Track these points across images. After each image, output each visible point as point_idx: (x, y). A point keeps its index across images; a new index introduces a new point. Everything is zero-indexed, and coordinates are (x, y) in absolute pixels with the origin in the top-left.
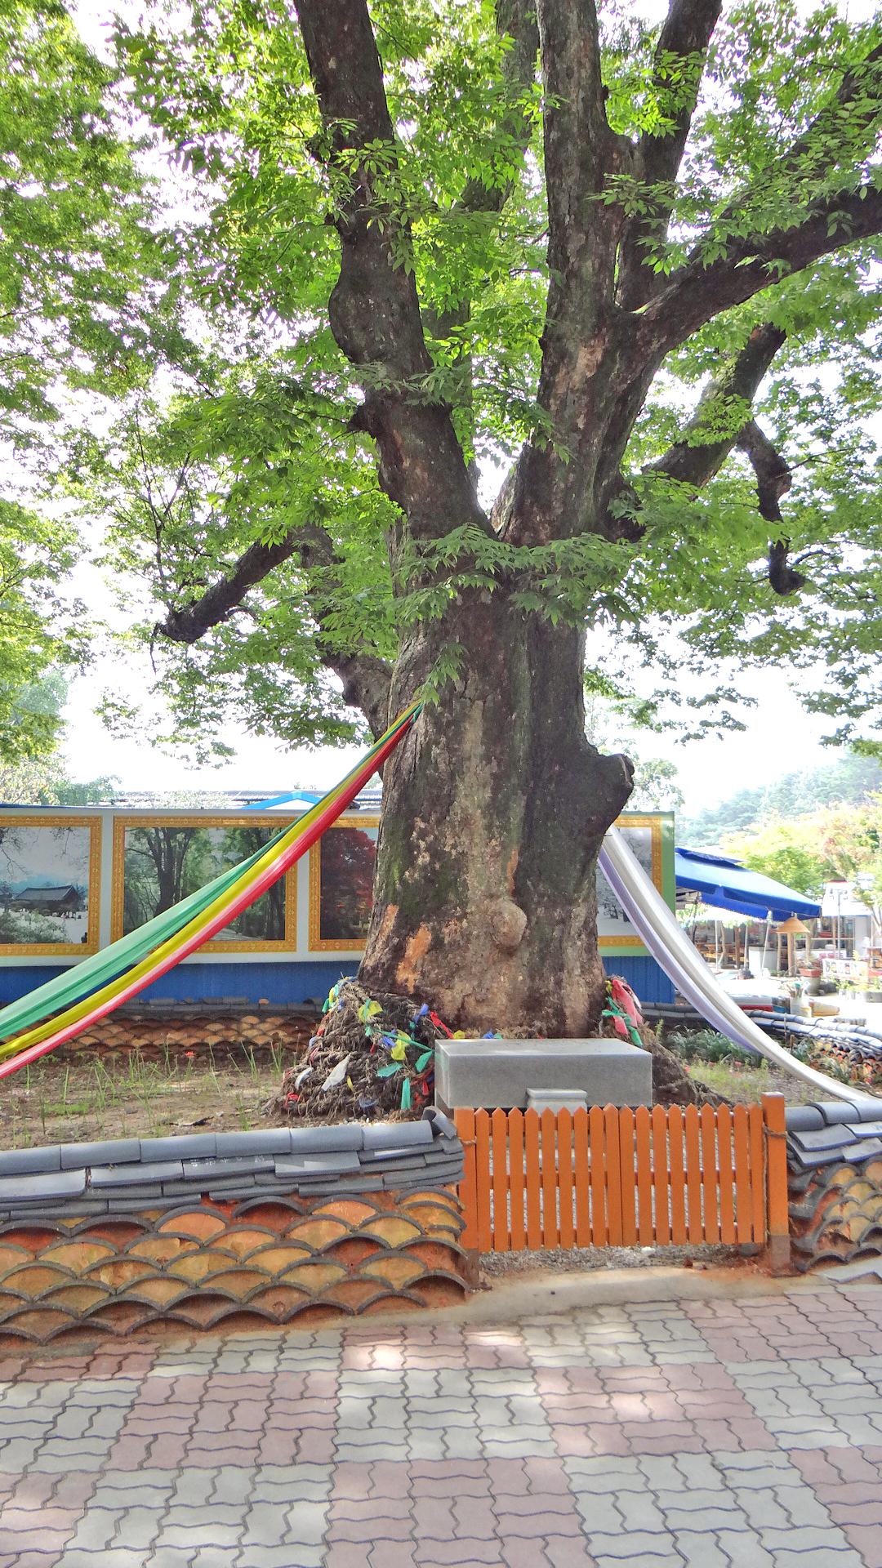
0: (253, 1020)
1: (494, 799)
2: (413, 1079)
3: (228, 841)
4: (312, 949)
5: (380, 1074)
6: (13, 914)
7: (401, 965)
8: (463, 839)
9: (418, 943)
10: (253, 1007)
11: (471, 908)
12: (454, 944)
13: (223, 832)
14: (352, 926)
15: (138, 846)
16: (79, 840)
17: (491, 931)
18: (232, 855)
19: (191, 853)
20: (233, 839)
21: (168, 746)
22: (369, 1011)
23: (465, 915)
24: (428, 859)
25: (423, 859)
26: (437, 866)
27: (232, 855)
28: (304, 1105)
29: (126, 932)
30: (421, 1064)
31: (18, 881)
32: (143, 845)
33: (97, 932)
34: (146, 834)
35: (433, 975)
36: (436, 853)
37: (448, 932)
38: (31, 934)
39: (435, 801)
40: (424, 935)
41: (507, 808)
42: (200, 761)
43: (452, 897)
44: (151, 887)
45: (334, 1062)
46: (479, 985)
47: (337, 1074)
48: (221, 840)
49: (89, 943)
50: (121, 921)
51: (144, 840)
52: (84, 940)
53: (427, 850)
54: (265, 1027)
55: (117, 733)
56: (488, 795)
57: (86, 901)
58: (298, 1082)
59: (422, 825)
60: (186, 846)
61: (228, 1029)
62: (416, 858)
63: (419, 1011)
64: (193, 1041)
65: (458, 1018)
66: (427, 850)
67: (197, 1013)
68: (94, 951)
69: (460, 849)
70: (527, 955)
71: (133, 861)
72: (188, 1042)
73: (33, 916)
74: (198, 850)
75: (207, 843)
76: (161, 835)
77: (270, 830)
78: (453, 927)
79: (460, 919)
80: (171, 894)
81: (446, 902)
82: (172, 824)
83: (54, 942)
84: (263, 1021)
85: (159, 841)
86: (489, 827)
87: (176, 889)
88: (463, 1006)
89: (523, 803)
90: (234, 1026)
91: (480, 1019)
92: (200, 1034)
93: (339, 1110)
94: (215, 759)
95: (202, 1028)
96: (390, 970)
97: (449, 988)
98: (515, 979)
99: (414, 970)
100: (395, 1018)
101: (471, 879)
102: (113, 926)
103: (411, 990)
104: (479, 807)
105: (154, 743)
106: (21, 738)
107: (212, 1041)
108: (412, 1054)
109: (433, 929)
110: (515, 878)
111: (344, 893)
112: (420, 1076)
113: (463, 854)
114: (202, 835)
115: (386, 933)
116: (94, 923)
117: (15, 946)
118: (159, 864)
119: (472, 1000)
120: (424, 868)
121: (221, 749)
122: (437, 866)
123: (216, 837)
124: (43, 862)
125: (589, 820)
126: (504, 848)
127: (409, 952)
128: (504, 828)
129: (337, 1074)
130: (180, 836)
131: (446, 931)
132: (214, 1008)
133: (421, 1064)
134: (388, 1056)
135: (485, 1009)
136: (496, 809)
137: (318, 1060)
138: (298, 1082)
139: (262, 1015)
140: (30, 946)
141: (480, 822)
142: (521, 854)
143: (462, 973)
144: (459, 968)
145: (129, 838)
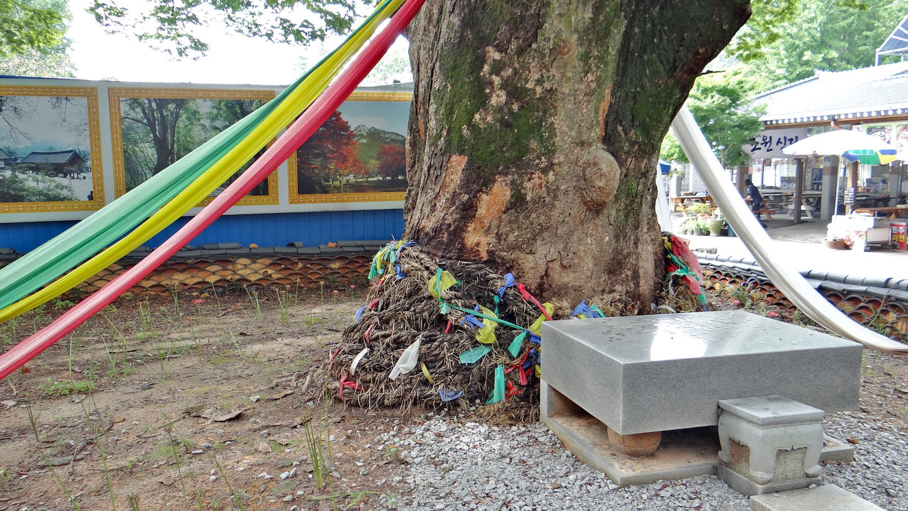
0: (246, 261)
1: (594, 20)
2: (508, 366)
3: (215, 111)
4: (292, 203)
5: (465, 359)
6: (21, 176)
7: (471, 227)
8: (553, 71)
9: (493, 200)
10: (245, 251)
11: (559, 158)
12: (538, 200)
13: (209, 103)
14: (324, 183)
15: (133, 115)
16: (76, 109)
17: (584, 181)
18: (219, 123)
19: (182, 122)
20: (219, 109)
21: (154, 42)
22: (442, 283)
23: (551, 166)
24: (503, 98)
25: (498, 98)
26: (515, 107)
27: (219, 123)
28: (366, 395)
29: (128, 189)
30: (515, 348)
31: (22, 147)
32: (138, 114)
33: (102, 191)
34: (140, 104)
35: (511, 238)
36: (514, 91)
37: (531, 188)
38: (40, 193)
39: (516, 25)
40: (501, 191)
41: (607, 33)
42: (180, 54)
43: (534, 144)
44: (149, 151)
45: (400, 344)
46: (565, 249)
47: (408, 359)
48: (208, 110)
49: (95, 200)
50: (123, 182)
51: (139, 110)
52: (91, 198)
53: (503, 87)
54: (256, 266)
55: (109, 29)
56: (589, 15)
57: (89, 163)
58: (354, 366)
59: (498, 56)
60: (178, 116)
61: (225, 269)
62: (488, 97)
63: (504, 282)
64: (196, 280)
65: (541, 286)
66: (503, 87)
67: (196, 258)
68: (101, 205)
69: (547, 85)
70: (613, 212)
71: (129, 128)
72: (191, 281)
73: (40, 177)
74: (188, 119)
75: (195, 113)
76: (154, 105)
77: (251, 103)
78: (537, 181)
79: (545, 171)
80: (166, 157)
81: (527, 150)
82: (163, 95)
83: (63, 199)
84: (254, 262)
85: (153, 111)
86: (585, 58)
87: (171, 153)
88: (546, 274)
89: (623, 29)
90: (230, 267)
91: (566, 286)
92: (201, 274)
93: (415, 404)
94: (192, 53)
95: (203, 270)
96: (458, 232)
97: (531, 253)
98: (602, 239)
99: (487, 232)
100: (474, 290)
101: (560, 122)
102: (116, 185)
103: (484, 256)
104: (576, 31)
105: (140, 38)
106: (23, 31)
107: (212, 279)
108: (503, 337)
109: (513, 183)
110: (606, 123)
111: (317, 156)
112: (516, 362)
113: (551, 91)
114: (192, 105)
115: (452, 187)
116: (98, 182)
117: (26, 204)
118: (153, 131)
119: (556, 266)
120: (500, 109)
121: (199, 46)
122: (515, 107)
123: (205, 107)
124: (45, 129)
125: (697, 53)
126: (599, 85)
127: (482, 211)
128: (601, 59)
129: (408, 359)
130: (171, 107)
131: (528, 185)
132: (212, 252)
133: (515, 348)
134: (472, 338)
135: (572, 275)
136: (596, 33)
137: (377, 339)
138: (354, 366)
139: (253, 257)
140: (40, 204)
141: (576, 50)
142: (613, 94)
143: (546, 235)
144: (542, 230)
145: (124, 108)
